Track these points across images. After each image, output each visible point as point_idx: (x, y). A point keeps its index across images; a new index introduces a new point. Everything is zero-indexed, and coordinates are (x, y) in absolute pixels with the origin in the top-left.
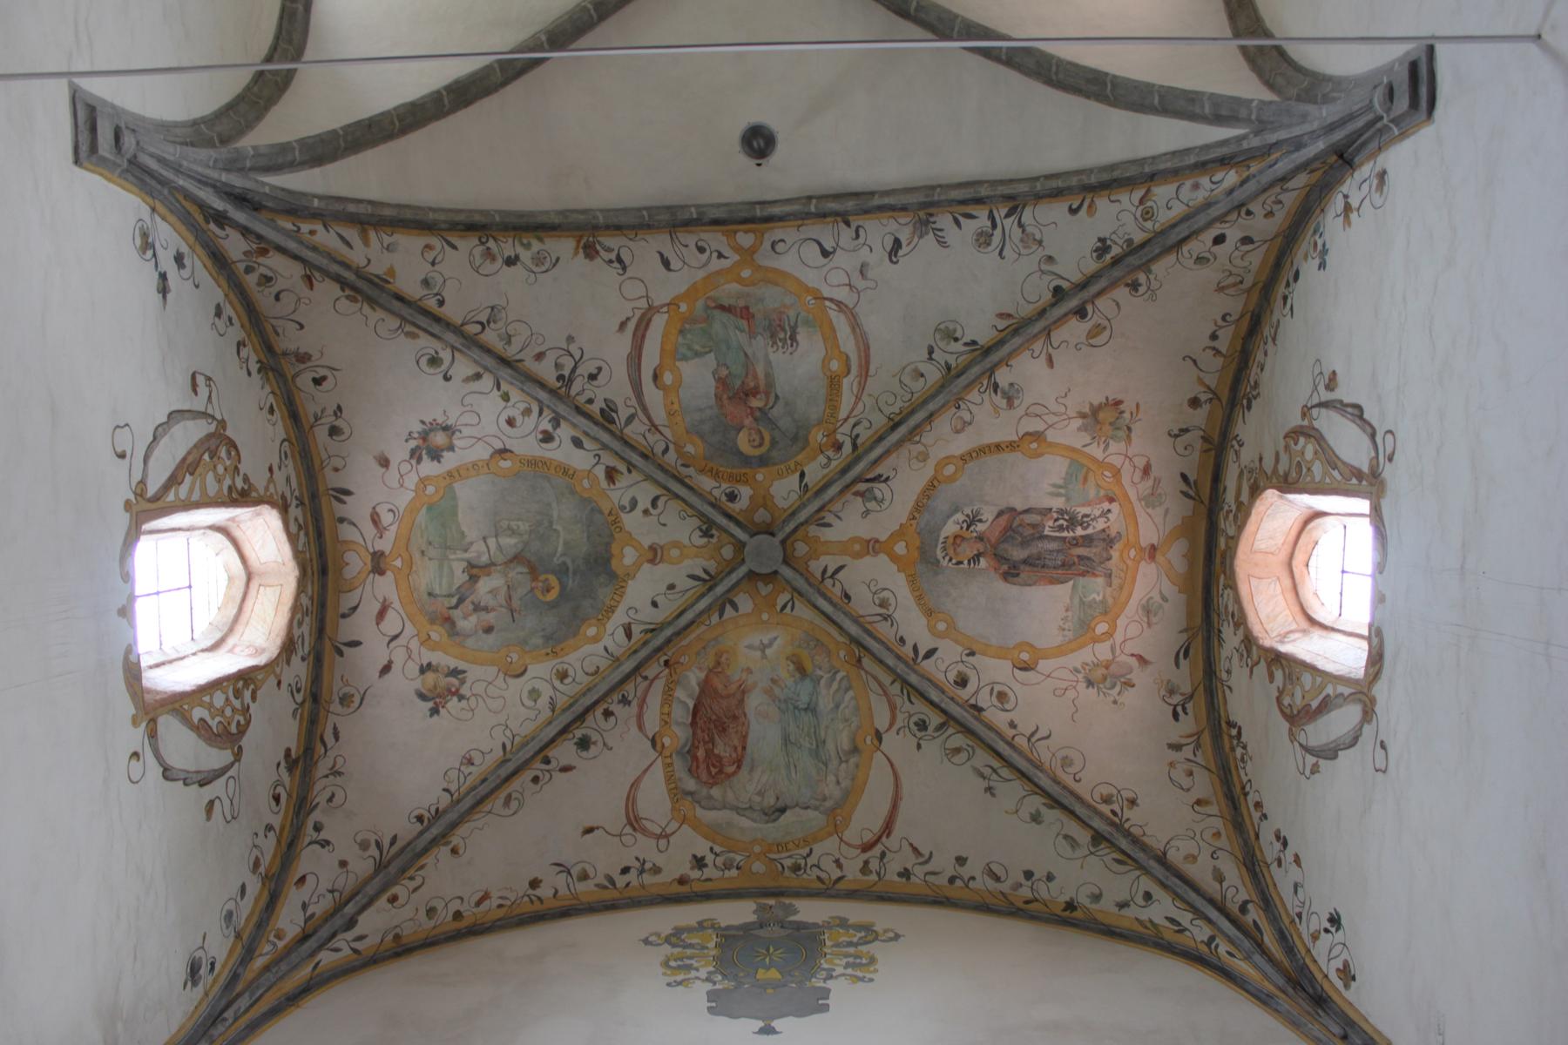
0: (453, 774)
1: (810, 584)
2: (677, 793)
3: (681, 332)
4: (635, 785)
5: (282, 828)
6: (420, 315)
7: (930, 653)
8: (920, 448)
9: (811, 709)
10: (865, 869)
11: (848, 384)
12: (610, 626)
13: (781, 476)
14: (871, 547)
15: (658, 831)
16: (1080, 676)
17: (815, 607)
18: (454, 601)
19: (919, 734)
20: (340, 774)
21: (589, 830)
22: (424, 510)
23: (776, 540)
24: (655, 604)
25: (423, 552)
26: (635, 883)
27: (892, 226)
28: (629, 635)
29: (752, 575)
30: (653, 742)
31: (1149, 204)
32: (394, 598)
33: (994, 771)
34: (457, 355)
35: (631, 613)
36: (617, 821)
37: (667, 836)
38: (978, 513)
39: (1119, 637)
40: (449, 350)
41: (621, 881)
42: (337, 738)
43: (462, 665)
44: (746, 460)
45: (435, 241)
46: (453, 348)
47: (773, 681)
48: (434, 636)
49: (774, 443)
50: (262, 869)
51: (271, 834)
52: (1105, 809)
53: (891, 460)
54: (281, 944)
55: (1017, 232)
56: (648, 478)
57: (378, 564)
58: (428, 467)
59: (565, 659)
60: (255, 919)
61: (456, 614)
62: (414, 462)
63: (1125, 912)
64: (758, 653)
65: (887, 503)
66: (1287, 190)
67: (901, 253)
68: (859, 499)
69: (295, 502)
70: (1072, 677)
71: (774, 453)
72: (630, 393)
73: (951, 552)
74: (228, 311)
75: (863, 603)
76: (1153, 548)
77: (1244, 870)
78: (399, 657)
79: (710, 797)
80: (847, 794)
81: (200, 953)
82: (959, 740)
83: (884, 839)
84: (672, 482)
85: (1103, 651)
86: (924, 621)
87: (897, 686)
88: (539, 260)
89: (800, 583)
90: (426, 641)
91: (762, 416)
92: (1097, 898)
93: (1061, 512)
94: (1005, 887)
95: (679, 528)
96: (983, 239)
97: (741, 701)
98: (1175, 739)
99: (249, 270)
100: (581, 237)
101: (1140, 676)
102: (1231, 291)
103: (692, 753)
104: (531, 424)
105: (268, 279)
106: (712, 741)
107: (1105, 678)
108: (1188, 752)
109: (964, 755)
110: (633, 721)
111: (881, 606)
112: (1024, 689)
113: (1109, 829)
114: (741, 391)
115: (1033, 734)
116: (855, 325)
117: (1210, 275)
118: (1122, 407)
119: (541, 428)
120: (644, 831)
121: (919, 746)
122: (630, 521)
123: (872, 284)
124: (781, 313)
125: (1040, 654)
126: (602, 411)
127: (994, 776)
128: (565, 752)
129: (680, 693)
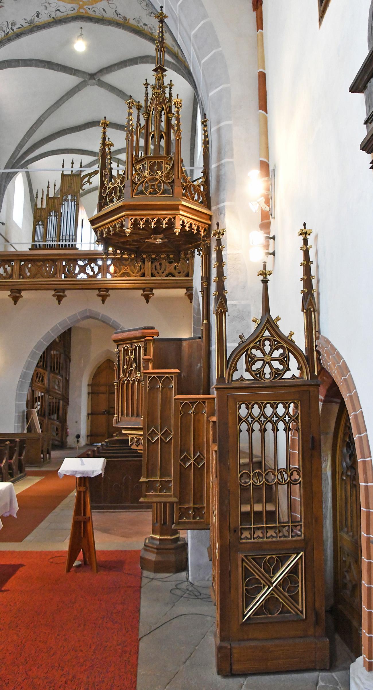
27: (40, 20)
55: (5, 29)
96: (13, 24)
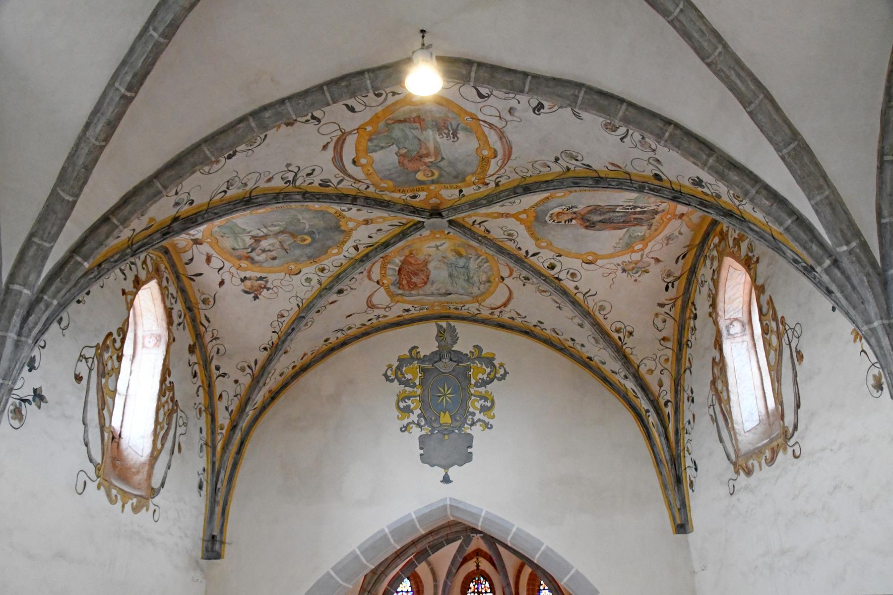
0: (275, 324)
12: (345, 248)
16: (619, 268)
18: (249, 250)
20: (218, 338)
32: (211, 251)
39: (647, 251)
42: (209, 321)
43: (264, 275)
52: (616, 336)
54: (224, 431)
61: (253, 255)
78: (227, 277)
85: (636, 257)
98: (663, 301)
107: (633, 269)
116: (502, 136)
125: (597, 257)
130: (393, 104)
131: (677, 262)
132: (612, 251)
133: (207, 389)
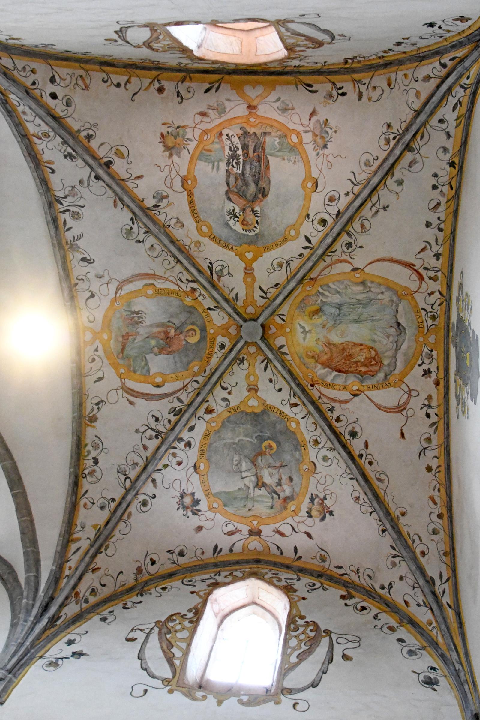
1: (269, 306)
2: (385, 384)
3: (135, 372)
4: (379, 407)
5: (379, 608)
6: (119, 511)
7: (308, 240)
8: (192, 246)
9: (339, 307)
10: (434, 279)
11: (160, 285)
12: (291, 415)
13: (211, 320)
14: (249, 271)
15: (406, 396)
16: (321, 152)
17: (281, 304)
19: (354, 247)
20: (358, 570)
21: (403, 435)
22: (227, 508)
23: (244, 325)
24: (280, 390)
25: (249, 510)
26: (436, 410)
27: (75, 262)
28: (296, 405)
29: (263, 338)
30: (355, 395)
31: (40, 135)
33: (374, 205)
34: (141, 492)
35: (284, 403)
36: (399, 418)
37: (410, 390)
38: (229, 212)
39: (299, 128)
40: (139, 496)
41: (434, 419)
43: (308, 496)
44: (203, 338)
45: (83, 501)
46: (137, 494)
47: (324, 327)
48: (293, 508)
49: (193, 324)
50: (395, 625)
51: (380, 616)
52: (392, 143)
53: (200, 261)
54: (434, 624)
55: (69, 199)
56: (211, 391)
57: (255, 533)
58: (203, 506)
59: (308, 440)
60: (418, 636)
61: (282, 495)
62: (200, 513)
63: (452, 134)
64: (308, 334)
65: (224, 264)
66: (15, 68)
67: (88, 258)
68: (222, 278)
69: (217, 577)
70: (322, 157)
71: (199, 323)
72: (166, 400)
73: (251, 227)
74: (105, 613)
75: (281, 276)
76: (249, 107)
77: (423, 63)
78: (303, 528)
79: (389, 365)
80: (389, 288)
81: (422, 677)
82: (356, 225)
83: (416, 268)
84: (215, 379)
85: (307, 138)
86: (289, 243)
87: (326, 258)
88: (96, 447)
89: (267, 313)
90: (296, 512)
91: (179, 330)
92: (445, 150)
93: (228, 164)
94: (443, 200)
95: (238, 376)
96: (76, 216)
97: (334, 345)
98: (356, 96)
99: (86, 601)
100: (86, 424)
101: (321, 116)
102: (88, 81)
103: (362, 375)
104: (181, 452)
105: (93, 590)
106: (356, 362)
107: (322, 137)
108: (363, 88)
109: (366, 223)
110: (343, 405)
111: (281, 267)
112: (327, 187)
113: (400, 145)
114: (166, 342)
115: (352, 182)
116: (128, 281)
117: (78, 97)
118: (165, 133)
119: (183, 447)
120: (406, 403)
121: (361, 247)
122: (234, 401)
123: (106, 272)
124: (125, 318)
125: (309, 176)
126: (175, 415)
127: (377, 205)
128: (357, 446)
129: (329, 379)
130: (105, 351)
131: (316, 92)
132: (301, 165)
133: (388, 609)
